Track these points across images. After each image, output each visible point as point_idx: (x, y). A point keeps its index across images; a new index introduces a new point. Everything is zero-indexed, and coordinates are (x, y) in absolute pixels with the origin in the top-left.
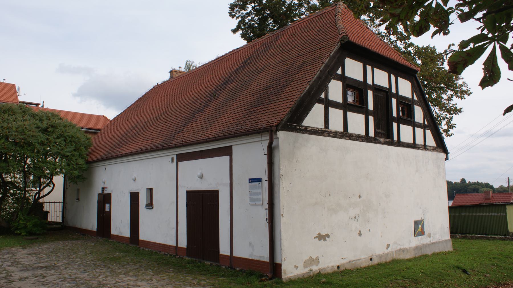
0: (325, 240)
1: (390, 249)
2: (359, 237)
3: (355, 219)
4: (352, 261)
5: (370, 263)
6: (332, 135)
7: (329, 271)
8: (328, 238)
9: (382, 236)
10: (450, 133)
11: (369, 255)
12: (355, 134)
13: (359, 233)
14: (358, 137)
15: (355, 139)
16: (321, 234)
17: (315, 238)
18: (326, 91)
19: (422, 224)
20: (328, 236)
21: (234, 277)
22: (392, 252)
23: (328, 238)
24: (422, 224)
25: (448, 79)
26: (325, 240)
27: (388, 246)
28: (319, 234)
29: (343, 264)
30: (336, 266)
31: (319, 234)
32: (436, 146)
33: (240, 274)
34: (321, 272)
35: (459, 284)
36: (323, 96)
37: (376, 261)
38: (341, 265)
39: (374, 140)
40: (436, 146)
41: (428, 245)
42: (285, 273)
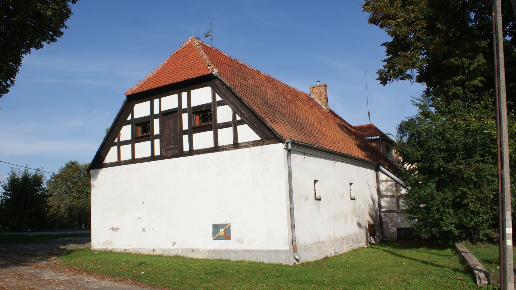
0: (116, 231)
1: (176, 247)
2: (143, 232)
3: (139, 219)
4: (136, 249)
5: (152, 253)
6: (122, 164)
7: (118, 251)
8: (118, 230)
9: (167, 234)
10: (325, 96)
11: (153, 247)
12: (141, 158)
13: (143, 230)
14: (144, 160)
15: (141, 161)
16: (114, 227)
17: (110, 229)
18: (119, 136)
19: (226, 227)
20: (118, 229)
21: (485, 193)
22: (178, 250)
23: (118, 230)
24: (226, 227)
25: (174, 148)
26: (116, 231)
27: (174, 243)
28: (112, 227)
29: (129, 249)
30: (123, 249)
31: (112, 227)
32: (260, 139)
33: (479, 182)
34: (113, 251)
35: (116, 257)
36: (116, 141)
37: (157, 253)
38: (127, 249)
39: (161, 157)
40: (260, 139)
41: (236, 251)
42: (93, 246)
